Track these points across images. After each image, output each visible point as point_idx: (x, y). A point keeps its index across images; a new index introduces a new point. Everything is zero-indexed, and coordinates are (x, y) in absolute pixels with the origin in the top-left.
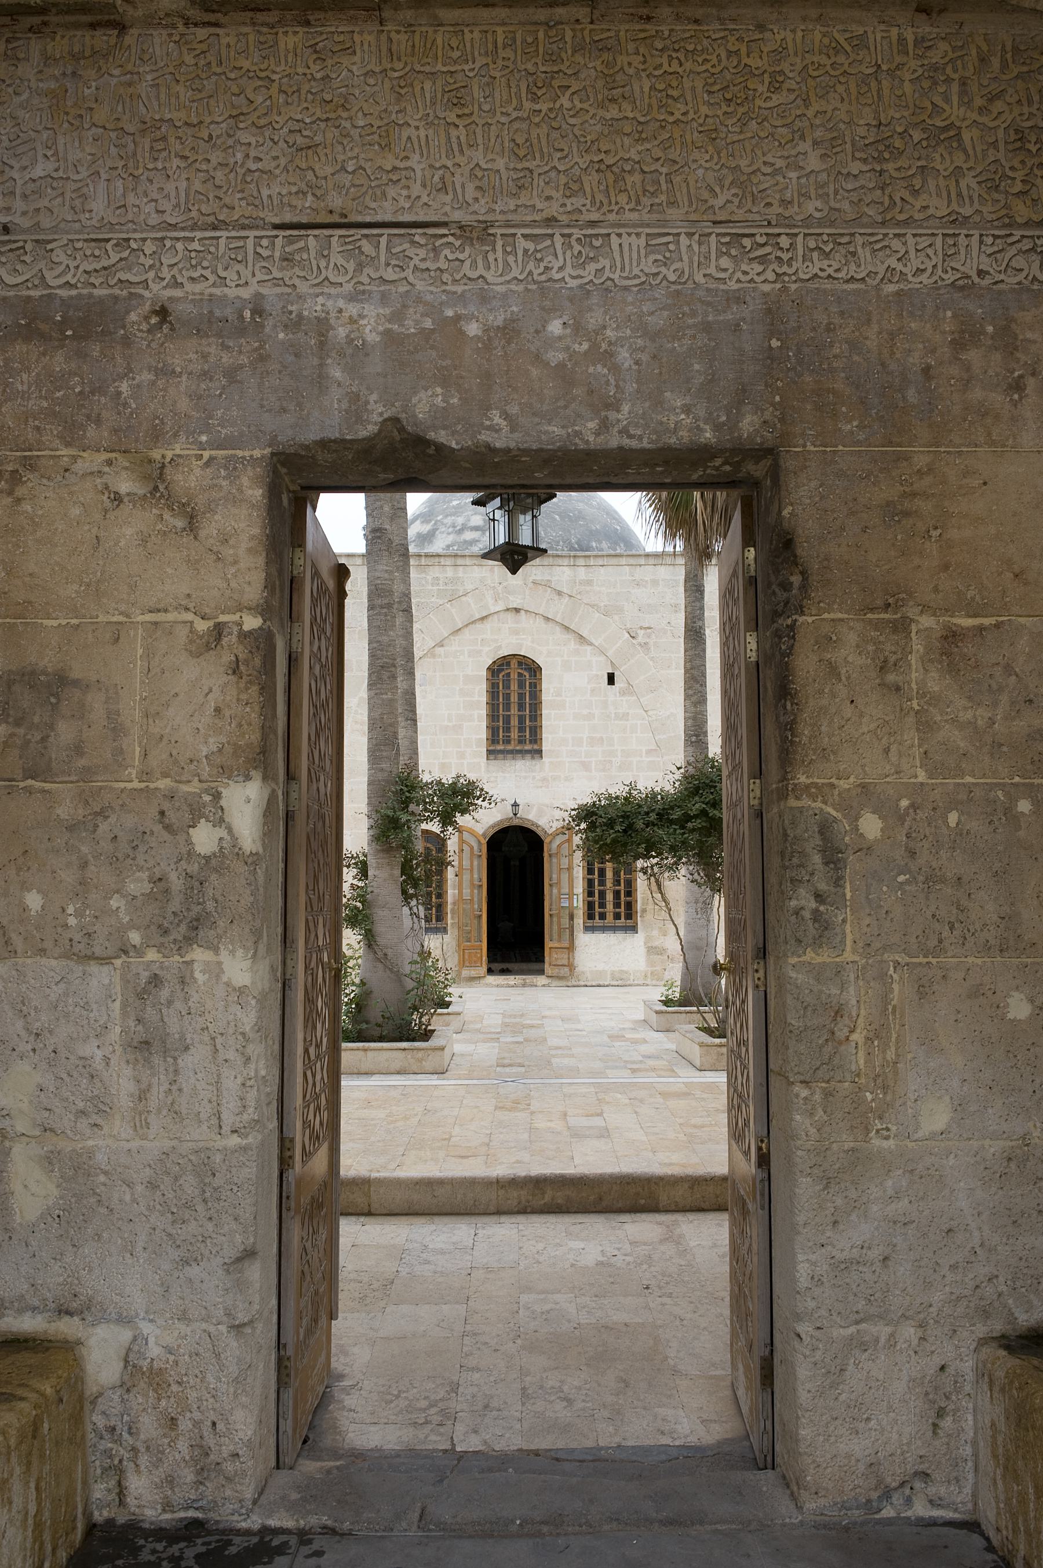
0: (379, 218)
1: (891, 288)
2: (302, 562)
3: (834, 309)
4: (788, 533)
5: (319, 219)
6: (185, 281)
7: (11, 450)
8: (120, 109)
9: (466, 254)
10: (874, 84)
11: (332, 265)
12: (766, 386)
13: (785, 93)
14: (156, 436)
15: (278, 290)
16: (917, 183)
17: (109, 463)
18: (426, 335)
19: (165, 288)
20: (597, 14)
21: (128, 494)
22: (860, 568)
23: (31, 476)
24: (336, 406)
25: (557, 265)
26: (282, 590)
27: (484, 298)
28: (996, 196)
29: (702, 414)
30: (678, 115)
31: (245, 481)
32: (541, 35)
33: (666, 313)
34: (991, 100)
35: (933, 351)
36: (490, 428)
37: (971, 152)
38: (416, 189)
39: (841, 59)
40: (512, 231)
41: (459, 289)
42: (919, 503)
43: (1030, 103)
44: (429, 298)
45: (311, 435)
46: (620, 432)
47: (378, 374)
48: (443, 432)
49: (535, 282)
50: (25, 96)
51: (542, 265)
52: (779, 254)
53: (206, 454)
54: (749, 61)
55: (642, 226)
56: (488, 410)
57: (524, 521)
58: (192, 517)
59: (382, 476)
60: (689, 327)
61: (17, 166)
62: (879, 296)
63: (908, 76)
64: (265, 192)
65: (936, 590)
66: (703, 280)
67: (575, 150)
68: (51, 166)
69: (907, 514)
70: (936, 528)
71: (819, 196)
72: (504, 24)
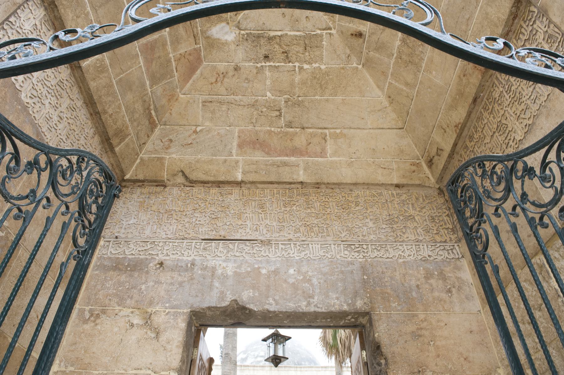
0: (236, 238)
1: (401, 261)
2: (196, 354)
3: (383, 267)
4: (378, 343)
5: (217, 238)
6: (170, 254)
7: (99, 307)
8: (160, 207)
9: (263, 249)
10: (386, 205)
11: (219, 251)
12: (364, 291)
13: (360, 207)
14: (151, 303)
15: (200, 258)
16: (404, 230)
17: (132, 312)
18: (248, 273)
19: (163, 256)
20: (303, 186)
21: (136, 324)
22: (407, 356)
23: (103, 316)
24: (215, 295)
25: (292, 252)
26: (187, 364)
27: (268, 262)
28: (429, 234)
29: (343, 300)
30: (328, 212)
31: (179, 320)
32: (287, 191)
33: (328, 268)
34: (422, 209)
35: (419, 280)
36: (268, 304)
37: (418, 222)
38: (248, 230)
39: (375, 198)
40: (278, 242)
41: (260, 259)
42: (423, 332)
43: (433, 209)
44: (250, 261)
45: (205, 305)
46: (314, 306)
47: (231, 285)
48: (252, 305)
49: (284, 257)
50: (133, 202)
51: (287, 252)
52: (363, 250)
53: (167, 311)
54: (348, 199)
55: (319, 242)
56: (268, 298)
57: (280, 347)
58: (158, 333)
59: (229, 321)
60: (336, 272)
61: (125, 220)
62: (398, 263)
63: (396, 203)
64: (200, 230)
65: (436, 365)
66: (340, 258)
67: (297, 220)
68: (136, 220)
69: (420, 336)
70: (432, 341)
71: (374, 234)
72: (277, 189)
